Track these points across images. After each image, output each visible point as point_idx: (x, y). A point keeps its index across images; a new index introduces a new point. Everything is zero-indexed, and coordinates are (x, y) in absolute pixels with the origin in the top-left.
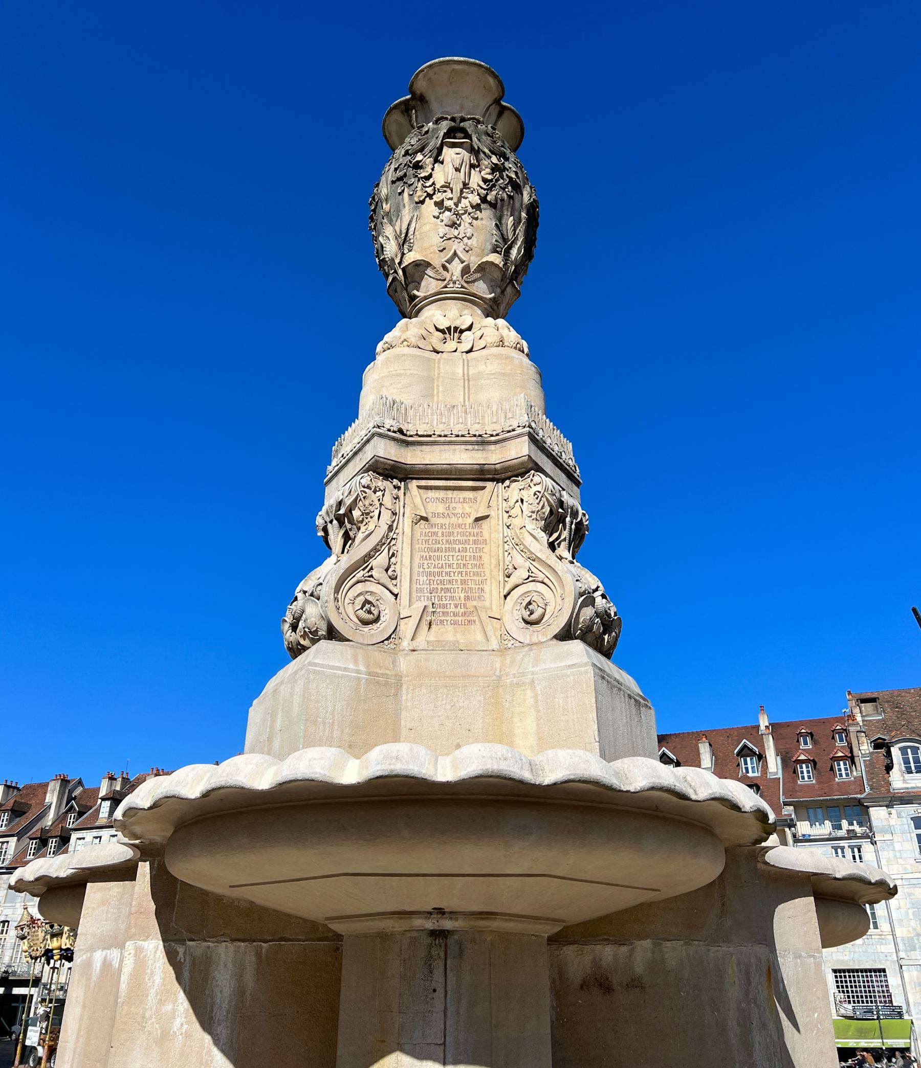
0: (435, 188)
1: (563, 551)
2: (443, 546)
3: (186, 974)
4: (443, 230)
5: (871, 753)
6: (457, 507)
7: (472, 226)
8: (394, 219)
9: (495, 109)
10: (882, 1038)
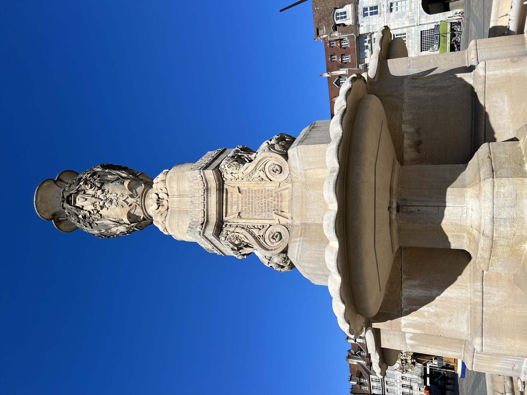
0: (94, 210)
1: (252, 156)
2: (250, 206)
3: (414, 307)
4: (113, 206)
5: (339, 32)
6: (234, 200)
7: (112, 193)
8: (109, 227)
9: (59, 183)
10: (447, 33)
